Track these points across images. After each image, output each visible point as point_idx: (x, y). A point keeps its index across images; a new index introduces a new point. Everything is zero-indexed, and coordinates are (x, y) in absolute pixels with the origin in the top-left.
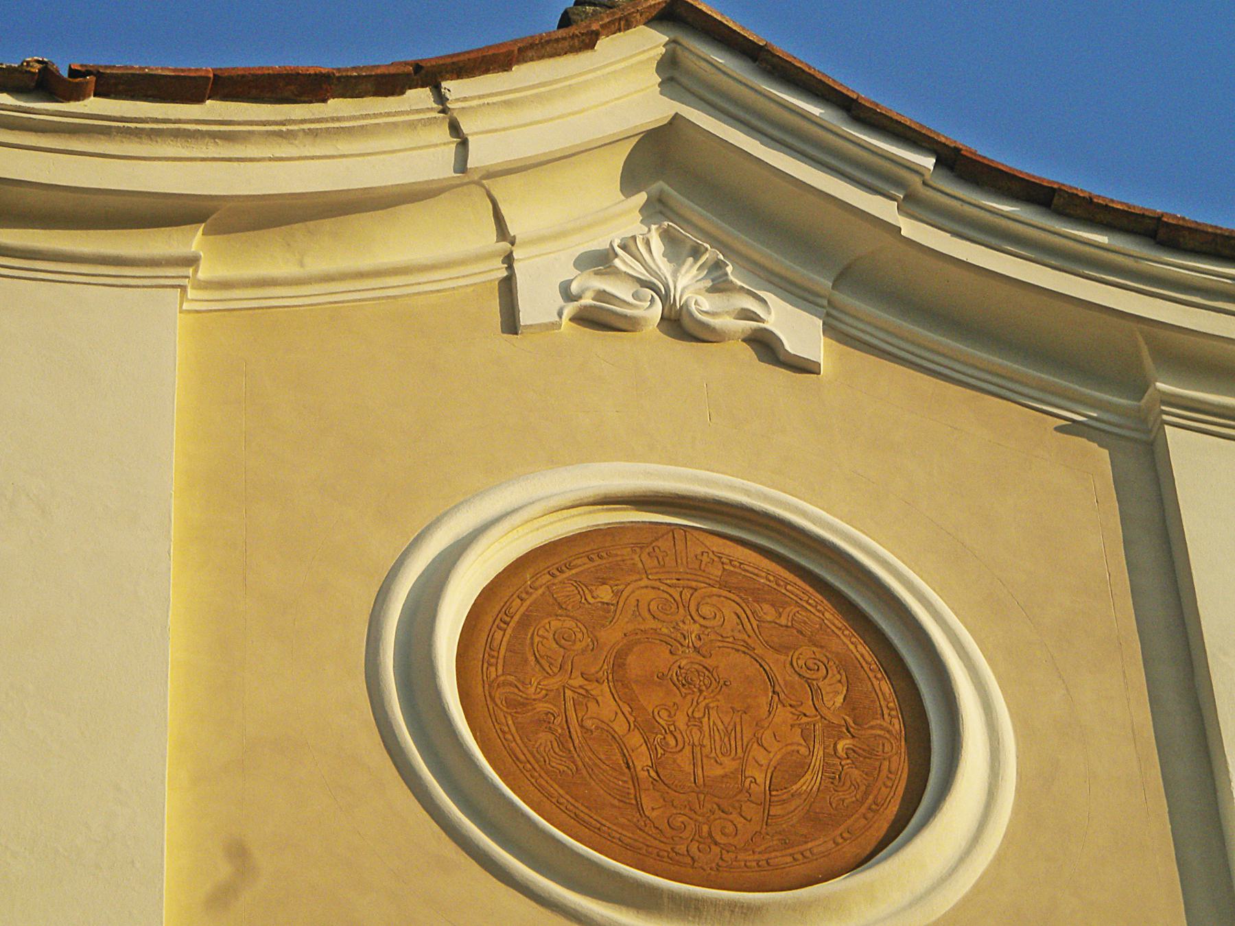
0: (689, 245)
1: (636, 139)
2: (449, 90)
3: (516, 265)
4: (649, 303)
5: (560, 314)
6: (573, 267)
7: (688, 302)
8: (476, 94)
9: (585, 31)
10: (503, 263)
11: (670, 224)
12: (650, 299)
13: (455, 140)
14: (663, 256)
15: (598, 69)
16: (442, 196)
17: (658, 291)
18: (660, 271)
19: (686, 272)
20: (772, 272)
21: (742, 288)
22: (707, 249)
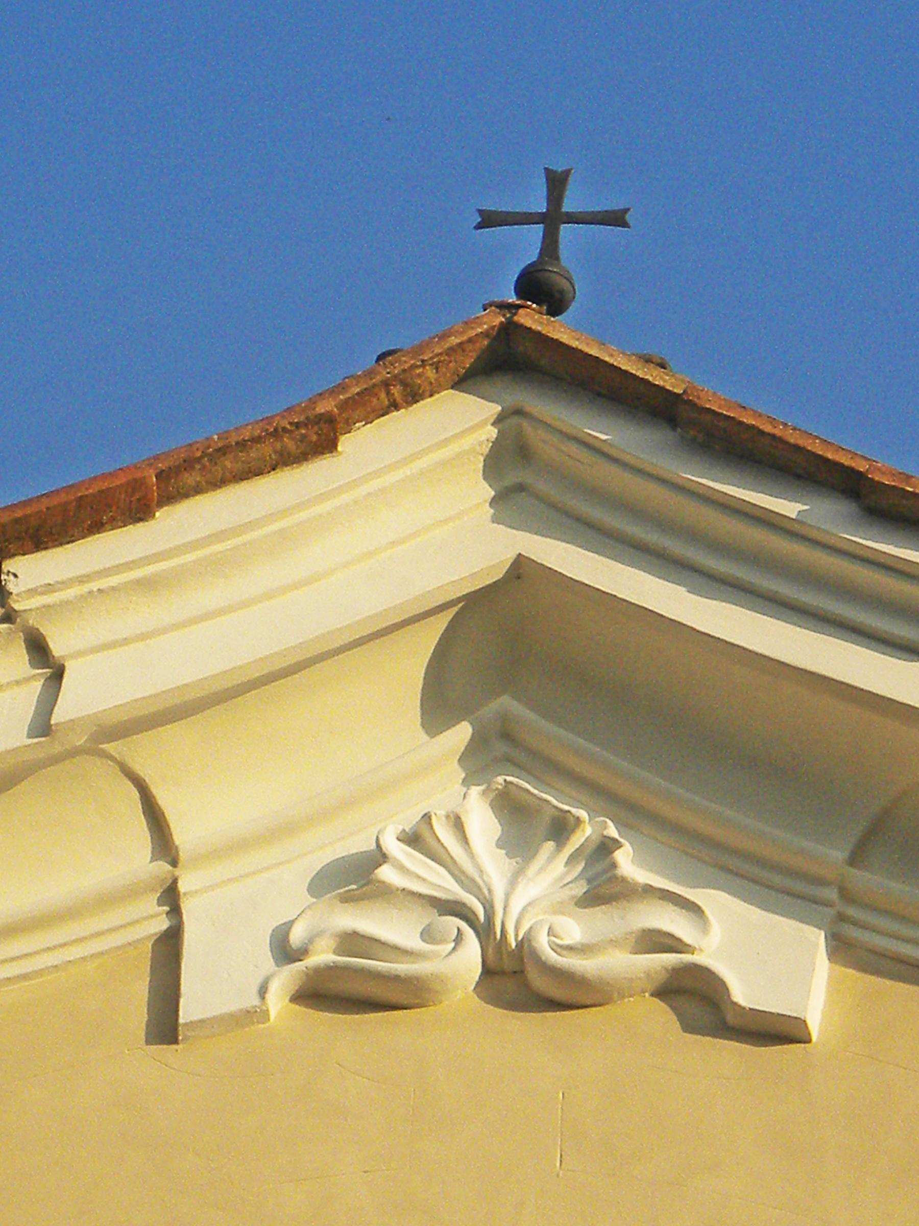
0: (547, 816)
1: (441, 622)
2: (15, 576)
3: (186, 906)
4: (453, 945)
5: (263, 991)
6: (307, 893)
7: (532, 934)
8: (71, 575)
9: (302, 418)
10: (160, 903)
11: (509, 778)
12: (454, 938)
13: (44, 671)
14: (498, 848)
15: (339, 490)
16: (25, 785)
17: (472, 917)
18: (481, 877)
19: (541, 870)
20: (718, 846)
21: (648, 890)
22: (578, 821)
